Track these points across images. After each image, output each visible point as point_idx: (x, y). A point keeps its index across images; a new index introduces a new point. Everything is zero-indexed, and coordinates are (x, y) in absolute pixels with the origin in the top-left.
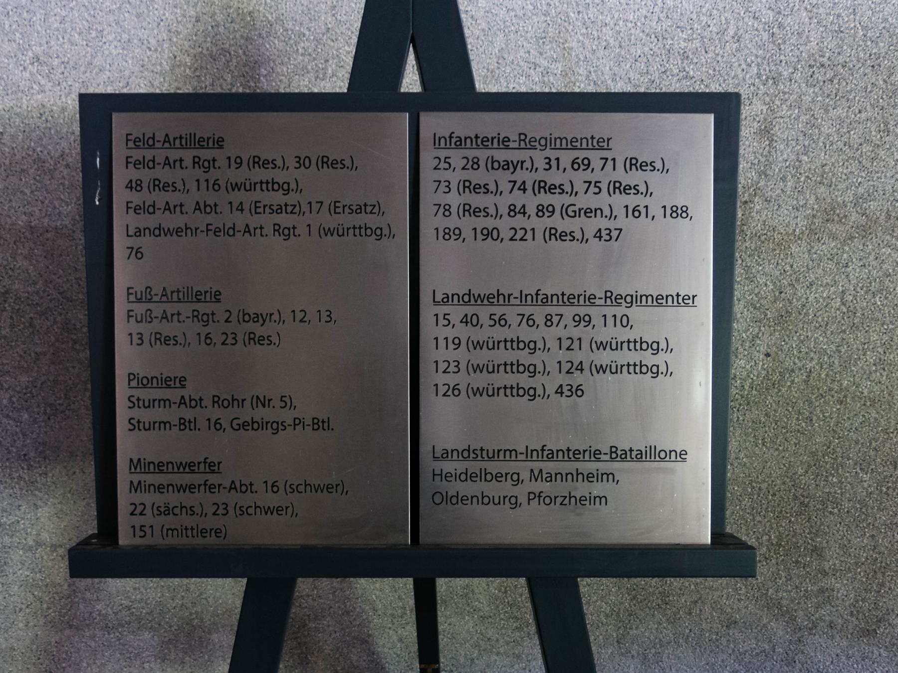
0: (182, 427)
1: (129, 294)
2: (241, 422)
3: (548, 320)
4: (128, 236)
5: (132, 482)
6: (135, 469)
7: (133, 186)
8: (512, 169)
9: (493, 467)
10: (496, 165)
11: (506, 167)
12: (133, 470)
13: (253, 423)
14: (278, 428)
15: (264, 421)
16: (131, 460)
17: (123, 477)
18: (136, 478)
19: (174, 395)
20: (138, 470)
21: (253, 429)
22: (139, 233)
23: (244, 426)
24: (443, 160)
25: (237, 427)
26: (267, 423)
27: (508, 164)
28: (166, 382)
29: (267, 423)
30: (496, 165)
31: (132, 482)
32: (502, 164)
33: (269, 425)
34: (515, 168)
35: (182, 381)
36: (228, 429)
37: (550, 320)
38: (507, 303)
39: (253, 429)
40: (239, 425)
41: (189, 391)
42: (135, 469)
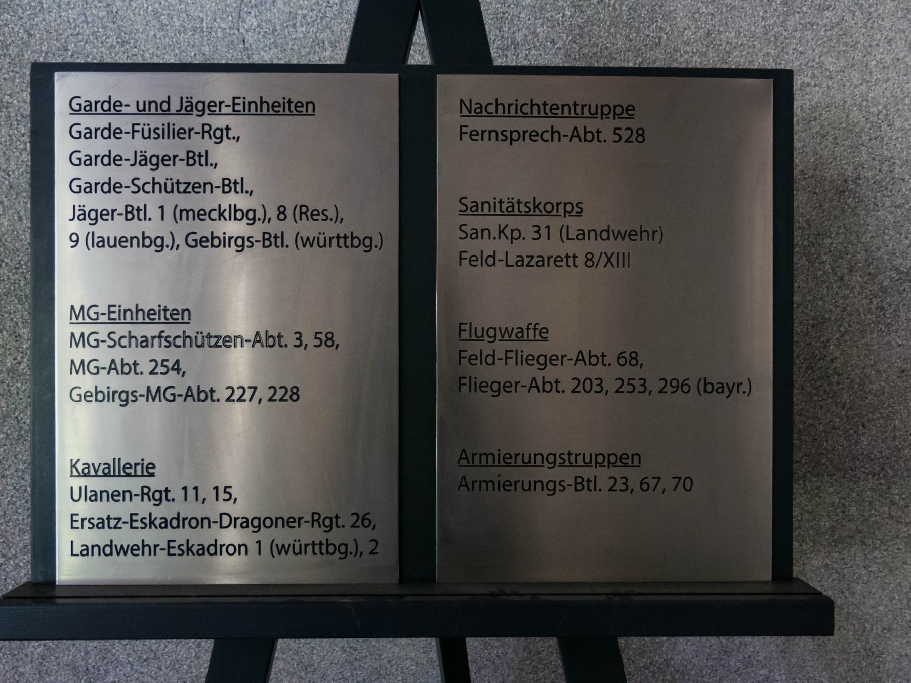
0: (130, 216)
1: (72, 521)
2: (198, 237)
3: (588, 259)
4: (72, 555)
5: (73, 335)
6: (77, 318)
7: (76, 134)
8: (727, 392)
9: (511, 474)
10: (709, 388)
11: (720, 390)
12: (74, 320)
13: (213, 238)
14: (243, 246)
15: (227, 236)
16: (73, 362)
17: (65, 483)
18: (78, 330)
19: (134, 484)
20: (80, 320)
21: (212, 246)
22: (86, 551)
23: (201, 242)
24: (626, 382)
25: (193, 244)
26: (230, 238)
27: (723, 387)
28: (127, 471)
29: (230, 238)
30: (709, 388)
31: (73, 335)
32: (716, 386)
33: (233, 241)
34: (731, 391)
35: (149, 470)
36: (183, 246)
37: (591, 260)
38: (506, 114)
39: (212, 246)
40: (195, 240)
41: (154, 483)
42: (77, 318)
